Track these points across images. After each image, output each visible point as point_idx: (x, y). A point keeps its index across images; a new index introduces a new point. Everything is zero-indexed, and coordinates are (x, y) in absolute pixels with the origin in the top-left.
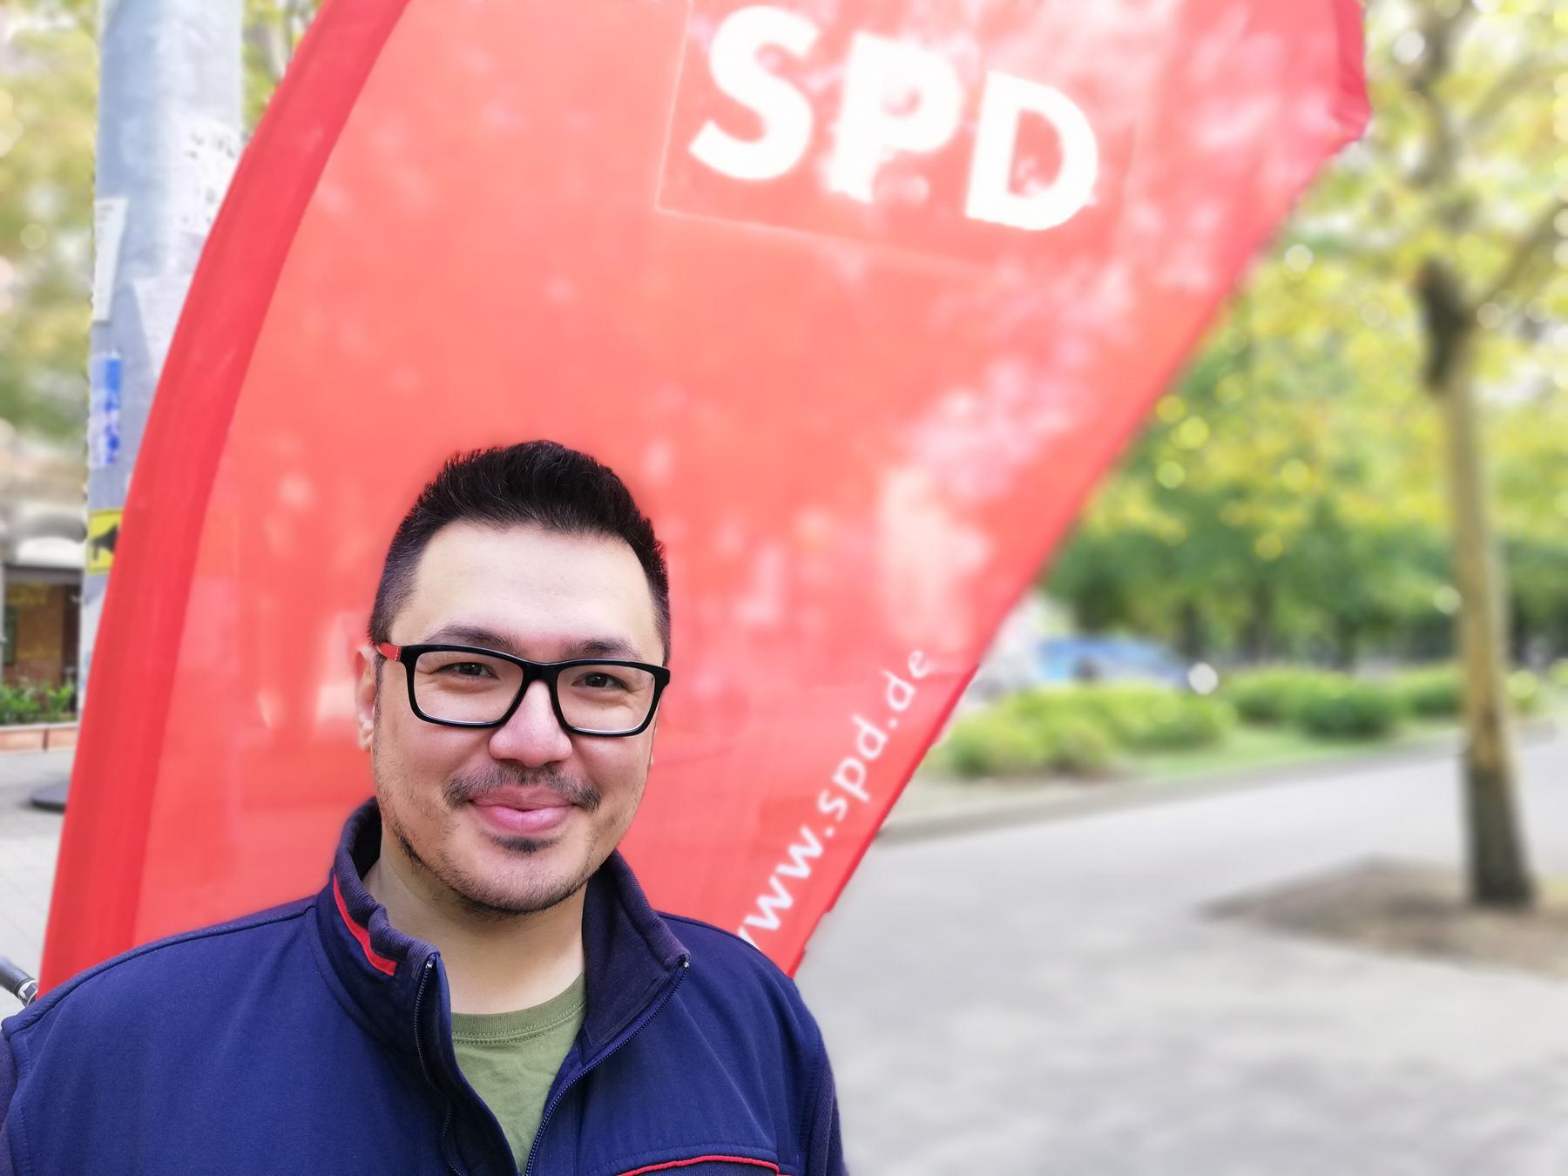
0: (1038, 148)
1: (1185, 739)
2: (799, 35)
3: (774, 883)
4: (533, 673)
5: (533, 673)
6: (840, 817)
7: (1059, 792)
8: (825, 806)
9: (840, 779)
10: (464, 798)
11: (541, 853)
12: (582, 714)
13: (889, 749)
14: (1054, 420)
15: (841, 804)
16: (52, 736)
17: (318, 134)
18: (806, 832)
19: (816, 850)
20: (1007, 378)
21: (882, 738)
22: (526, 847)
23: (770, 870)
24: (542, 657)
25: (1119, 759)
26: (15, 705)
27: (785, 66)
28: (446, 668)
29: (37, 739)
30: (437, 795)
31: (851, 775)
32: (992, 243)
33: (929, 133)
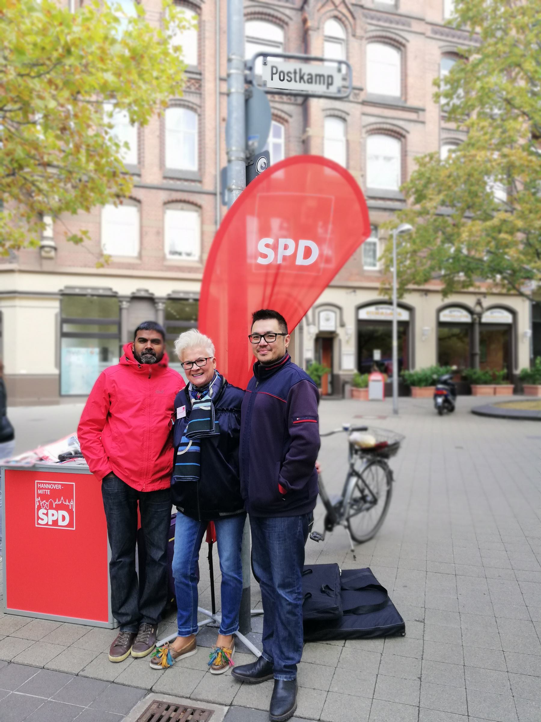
4: (262, 336)
5: (262, 336)
10: (258, 351)
12: (268, 340)
16: (498, 390)
17: (328, 171)
22: (264, 355)
24: (262, 334)
26: (483, 378)
28: (255, 337)
29: (492, 391)
30: (256, 352)
32: (302, 268)
33: (290, 252)
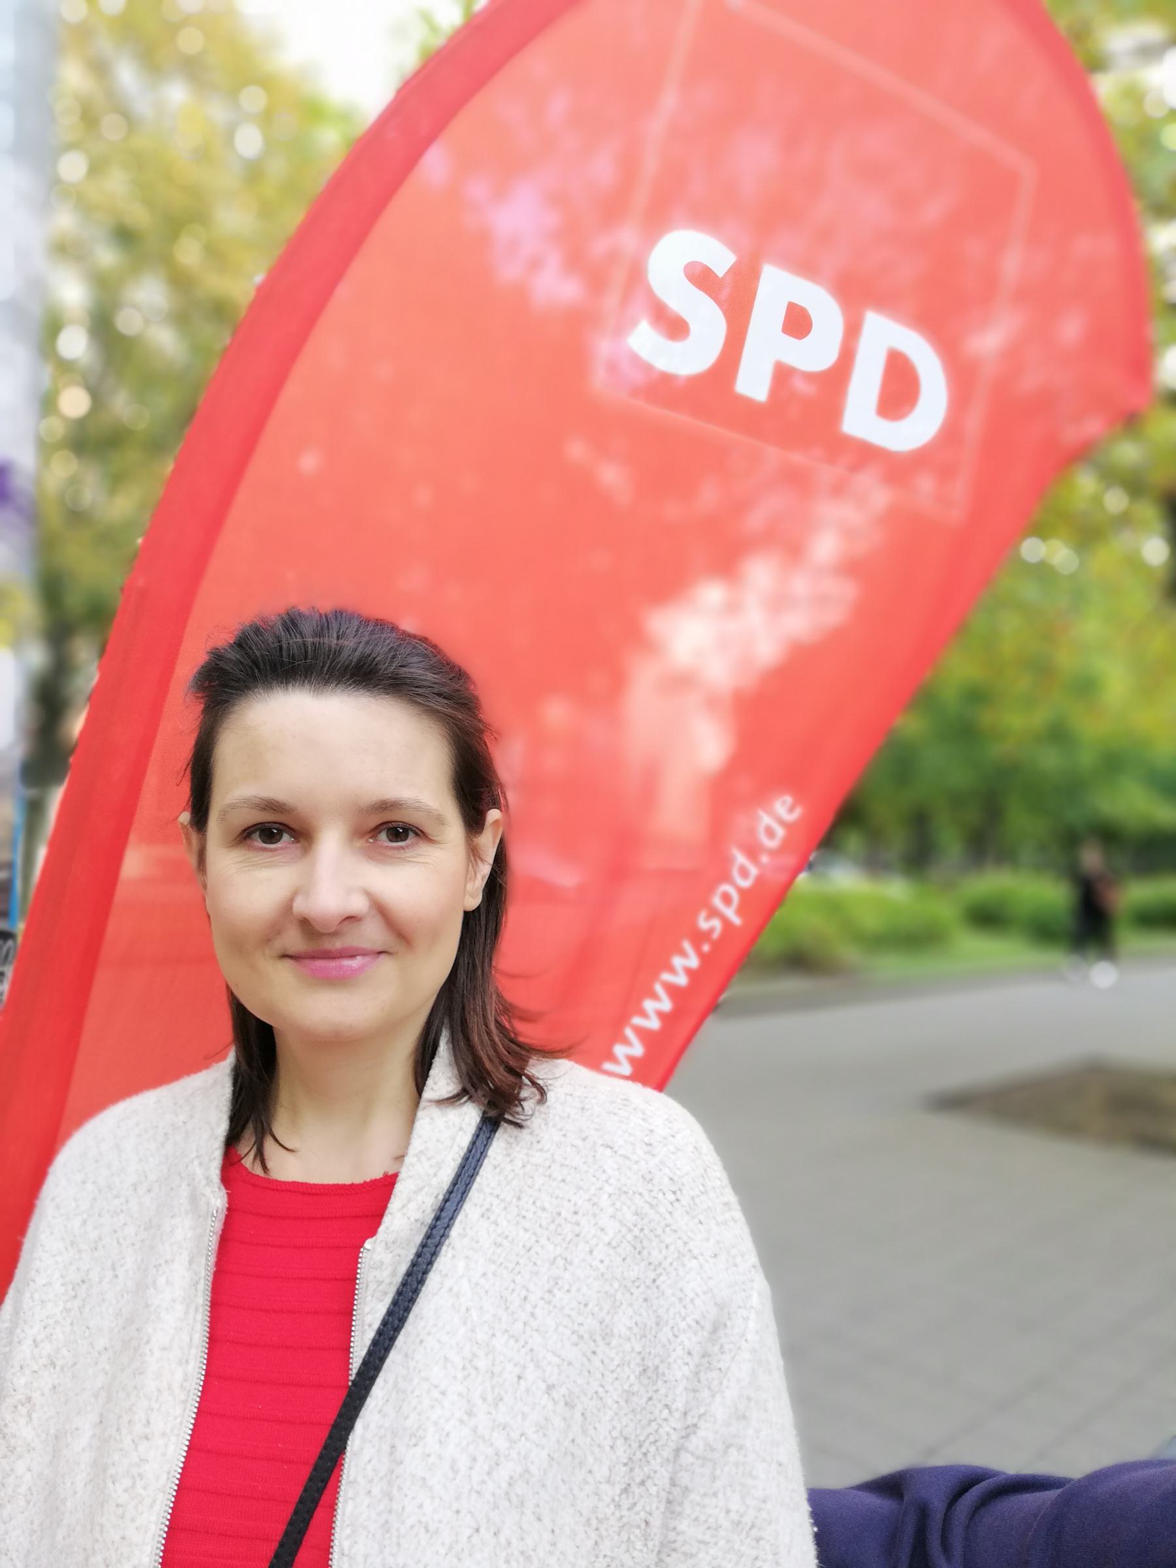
0: (899, 390)
1: (917, 939)
2: (720, 258)
3: (659, 989)
6: (716, 935)
7: (793, 984)
8: (704, 924)
9: (717, 901)
11: (829, 817)
13: (759, 880)
14: (800, 624)
15: (716, 924)
18: (687, 946)
19: (693, 962)
20: (760, 573)
21: (754, 871)
23: (655, 976)
25: (849, 953)
27: (701, 277)
31: (727, 899)
33: (815, 354)
